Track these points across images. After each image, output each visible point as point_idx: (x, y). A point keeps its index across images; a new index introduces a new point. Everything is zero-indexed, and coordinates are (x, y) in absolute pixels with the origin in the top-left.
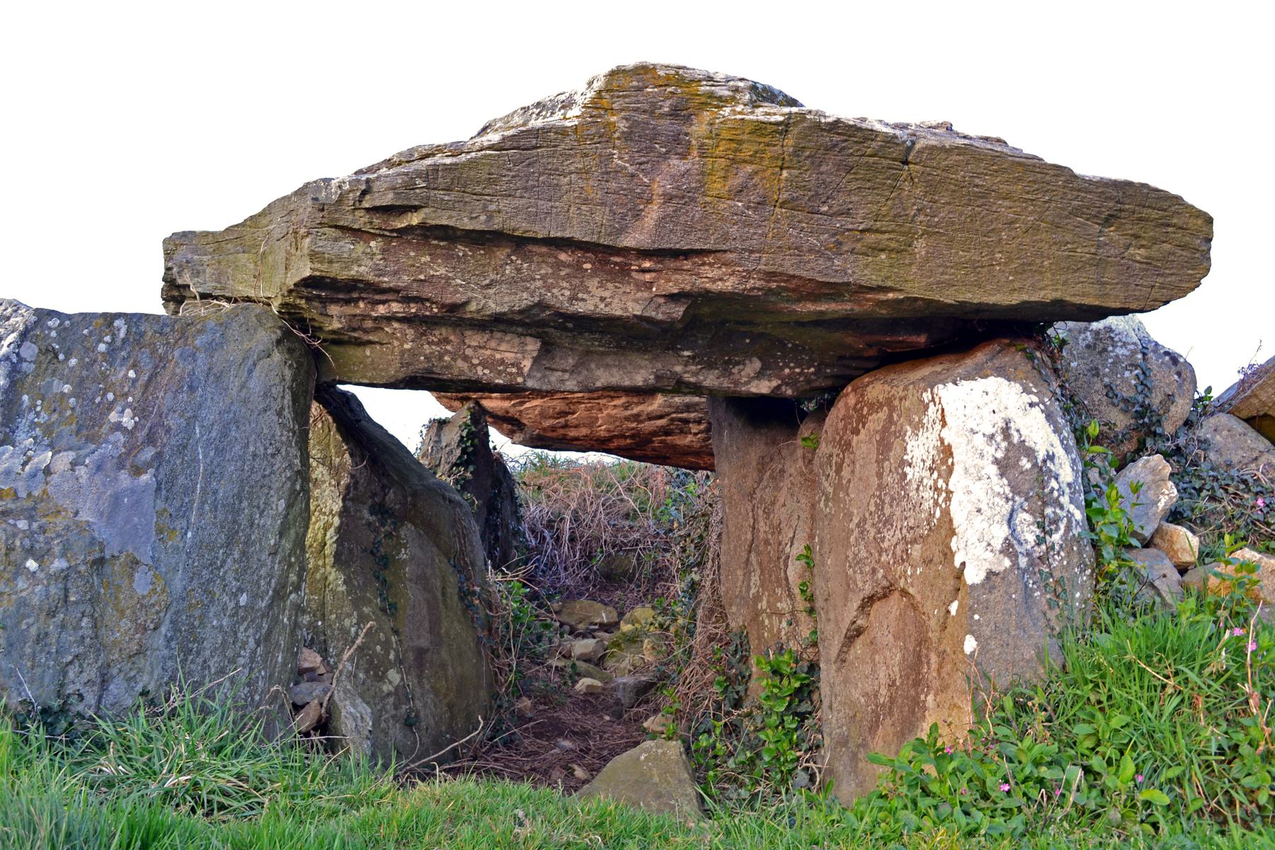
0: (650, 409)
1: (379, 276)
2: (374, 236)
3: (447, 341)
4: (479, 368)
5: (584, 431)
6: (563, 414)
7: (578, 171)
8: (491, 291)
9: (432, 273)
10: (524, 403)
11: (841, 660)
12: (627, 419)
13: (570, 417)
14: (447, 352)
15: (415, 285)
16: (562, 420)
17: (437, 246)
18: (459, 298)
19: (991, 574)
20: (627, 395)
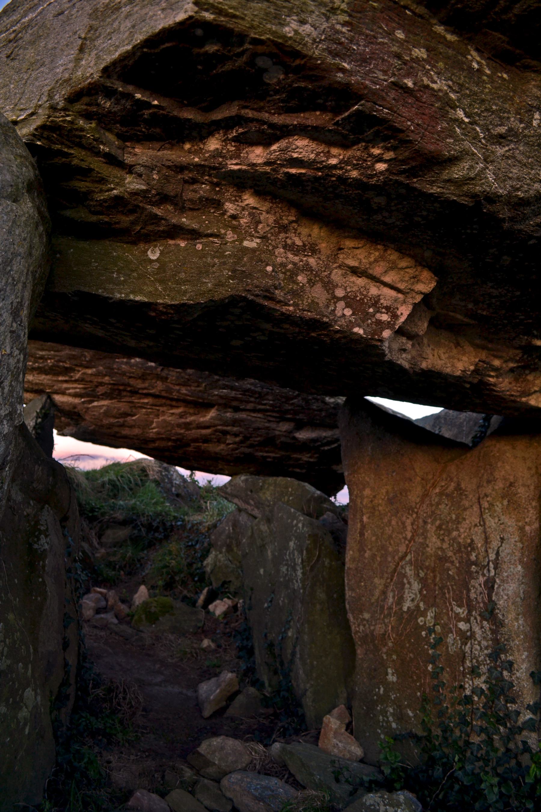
0: (202, 419)
1: (335, 54)
3: (314, 250)
4: (341, 305)
5: (136, 431)
6: (126, 415)
8: (500, 151)
9: (426, 81)
10: (93, 401)
12: (179, 426)
13: (129, 419)
14: (307, 268)
15: (392, 94)
16: (121, 420)
17: (442, 39)
18: (449, 147)
20: (186, 407)
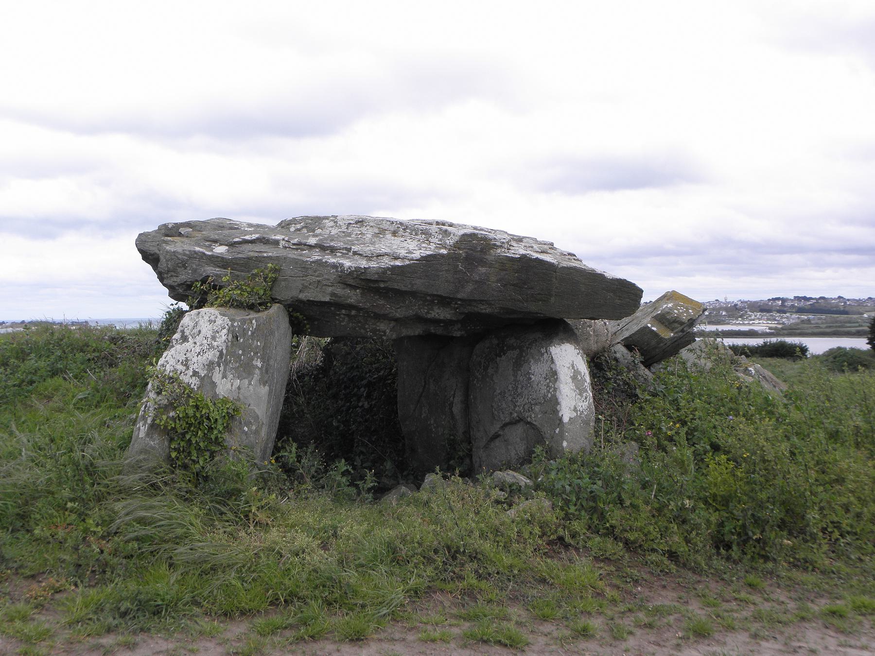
2: (358, 288)
7: (446, 271)
11: (486, 447)
19: (570, 418)
